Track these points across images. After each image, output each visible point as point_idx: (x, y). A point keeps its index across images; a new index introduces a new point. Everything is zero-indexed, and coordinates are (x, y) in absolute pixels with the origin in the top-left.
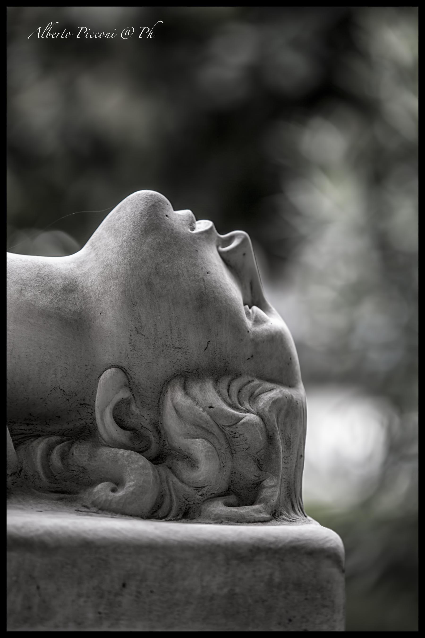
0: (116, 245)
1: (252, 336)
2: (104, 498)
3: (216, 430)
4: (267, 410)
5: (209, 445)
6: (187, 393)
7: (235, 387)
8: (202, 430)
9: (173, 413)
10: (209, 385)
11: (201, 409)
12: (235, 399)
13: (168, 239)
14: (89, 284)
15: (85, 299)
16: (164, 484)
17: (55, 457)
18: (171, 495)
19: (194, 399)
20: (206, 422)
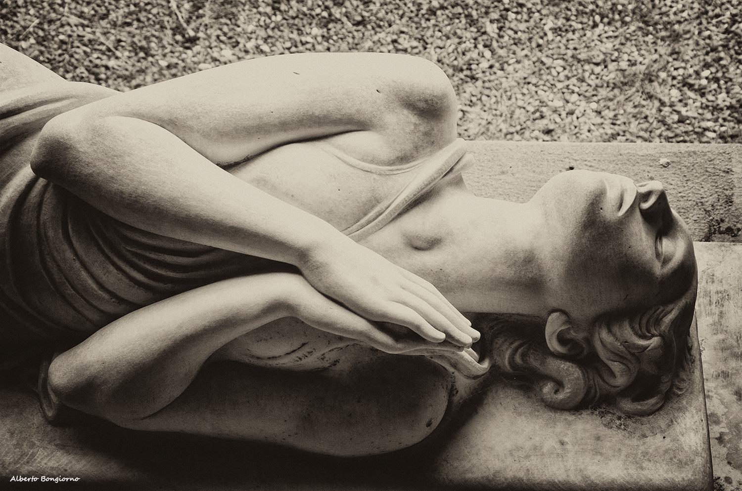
0: (562, 234)
1: (659, 280)
2: (550, 400)
3: (629, 357)
4: (667, 331)
5: (624, 367)
6: (610, 331)
7: (644, 321)
8: (620, 357)
9: (599, 342)
10: (626, 325)
11: (619, 344)
12: (644, 330)
13: (601, 230)
14: (542, 257)
15: (540, 268)
16: (592, 382)
17: (518, 359)
18: (596, 388)
19: (614, 335)
20: (622, 352)
